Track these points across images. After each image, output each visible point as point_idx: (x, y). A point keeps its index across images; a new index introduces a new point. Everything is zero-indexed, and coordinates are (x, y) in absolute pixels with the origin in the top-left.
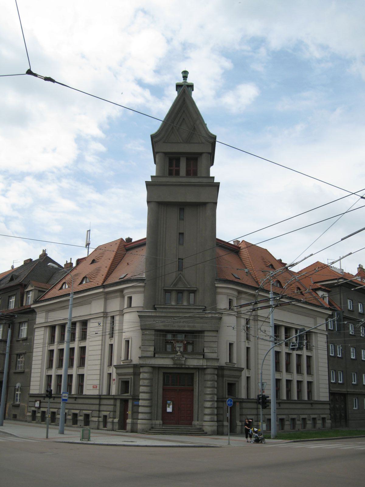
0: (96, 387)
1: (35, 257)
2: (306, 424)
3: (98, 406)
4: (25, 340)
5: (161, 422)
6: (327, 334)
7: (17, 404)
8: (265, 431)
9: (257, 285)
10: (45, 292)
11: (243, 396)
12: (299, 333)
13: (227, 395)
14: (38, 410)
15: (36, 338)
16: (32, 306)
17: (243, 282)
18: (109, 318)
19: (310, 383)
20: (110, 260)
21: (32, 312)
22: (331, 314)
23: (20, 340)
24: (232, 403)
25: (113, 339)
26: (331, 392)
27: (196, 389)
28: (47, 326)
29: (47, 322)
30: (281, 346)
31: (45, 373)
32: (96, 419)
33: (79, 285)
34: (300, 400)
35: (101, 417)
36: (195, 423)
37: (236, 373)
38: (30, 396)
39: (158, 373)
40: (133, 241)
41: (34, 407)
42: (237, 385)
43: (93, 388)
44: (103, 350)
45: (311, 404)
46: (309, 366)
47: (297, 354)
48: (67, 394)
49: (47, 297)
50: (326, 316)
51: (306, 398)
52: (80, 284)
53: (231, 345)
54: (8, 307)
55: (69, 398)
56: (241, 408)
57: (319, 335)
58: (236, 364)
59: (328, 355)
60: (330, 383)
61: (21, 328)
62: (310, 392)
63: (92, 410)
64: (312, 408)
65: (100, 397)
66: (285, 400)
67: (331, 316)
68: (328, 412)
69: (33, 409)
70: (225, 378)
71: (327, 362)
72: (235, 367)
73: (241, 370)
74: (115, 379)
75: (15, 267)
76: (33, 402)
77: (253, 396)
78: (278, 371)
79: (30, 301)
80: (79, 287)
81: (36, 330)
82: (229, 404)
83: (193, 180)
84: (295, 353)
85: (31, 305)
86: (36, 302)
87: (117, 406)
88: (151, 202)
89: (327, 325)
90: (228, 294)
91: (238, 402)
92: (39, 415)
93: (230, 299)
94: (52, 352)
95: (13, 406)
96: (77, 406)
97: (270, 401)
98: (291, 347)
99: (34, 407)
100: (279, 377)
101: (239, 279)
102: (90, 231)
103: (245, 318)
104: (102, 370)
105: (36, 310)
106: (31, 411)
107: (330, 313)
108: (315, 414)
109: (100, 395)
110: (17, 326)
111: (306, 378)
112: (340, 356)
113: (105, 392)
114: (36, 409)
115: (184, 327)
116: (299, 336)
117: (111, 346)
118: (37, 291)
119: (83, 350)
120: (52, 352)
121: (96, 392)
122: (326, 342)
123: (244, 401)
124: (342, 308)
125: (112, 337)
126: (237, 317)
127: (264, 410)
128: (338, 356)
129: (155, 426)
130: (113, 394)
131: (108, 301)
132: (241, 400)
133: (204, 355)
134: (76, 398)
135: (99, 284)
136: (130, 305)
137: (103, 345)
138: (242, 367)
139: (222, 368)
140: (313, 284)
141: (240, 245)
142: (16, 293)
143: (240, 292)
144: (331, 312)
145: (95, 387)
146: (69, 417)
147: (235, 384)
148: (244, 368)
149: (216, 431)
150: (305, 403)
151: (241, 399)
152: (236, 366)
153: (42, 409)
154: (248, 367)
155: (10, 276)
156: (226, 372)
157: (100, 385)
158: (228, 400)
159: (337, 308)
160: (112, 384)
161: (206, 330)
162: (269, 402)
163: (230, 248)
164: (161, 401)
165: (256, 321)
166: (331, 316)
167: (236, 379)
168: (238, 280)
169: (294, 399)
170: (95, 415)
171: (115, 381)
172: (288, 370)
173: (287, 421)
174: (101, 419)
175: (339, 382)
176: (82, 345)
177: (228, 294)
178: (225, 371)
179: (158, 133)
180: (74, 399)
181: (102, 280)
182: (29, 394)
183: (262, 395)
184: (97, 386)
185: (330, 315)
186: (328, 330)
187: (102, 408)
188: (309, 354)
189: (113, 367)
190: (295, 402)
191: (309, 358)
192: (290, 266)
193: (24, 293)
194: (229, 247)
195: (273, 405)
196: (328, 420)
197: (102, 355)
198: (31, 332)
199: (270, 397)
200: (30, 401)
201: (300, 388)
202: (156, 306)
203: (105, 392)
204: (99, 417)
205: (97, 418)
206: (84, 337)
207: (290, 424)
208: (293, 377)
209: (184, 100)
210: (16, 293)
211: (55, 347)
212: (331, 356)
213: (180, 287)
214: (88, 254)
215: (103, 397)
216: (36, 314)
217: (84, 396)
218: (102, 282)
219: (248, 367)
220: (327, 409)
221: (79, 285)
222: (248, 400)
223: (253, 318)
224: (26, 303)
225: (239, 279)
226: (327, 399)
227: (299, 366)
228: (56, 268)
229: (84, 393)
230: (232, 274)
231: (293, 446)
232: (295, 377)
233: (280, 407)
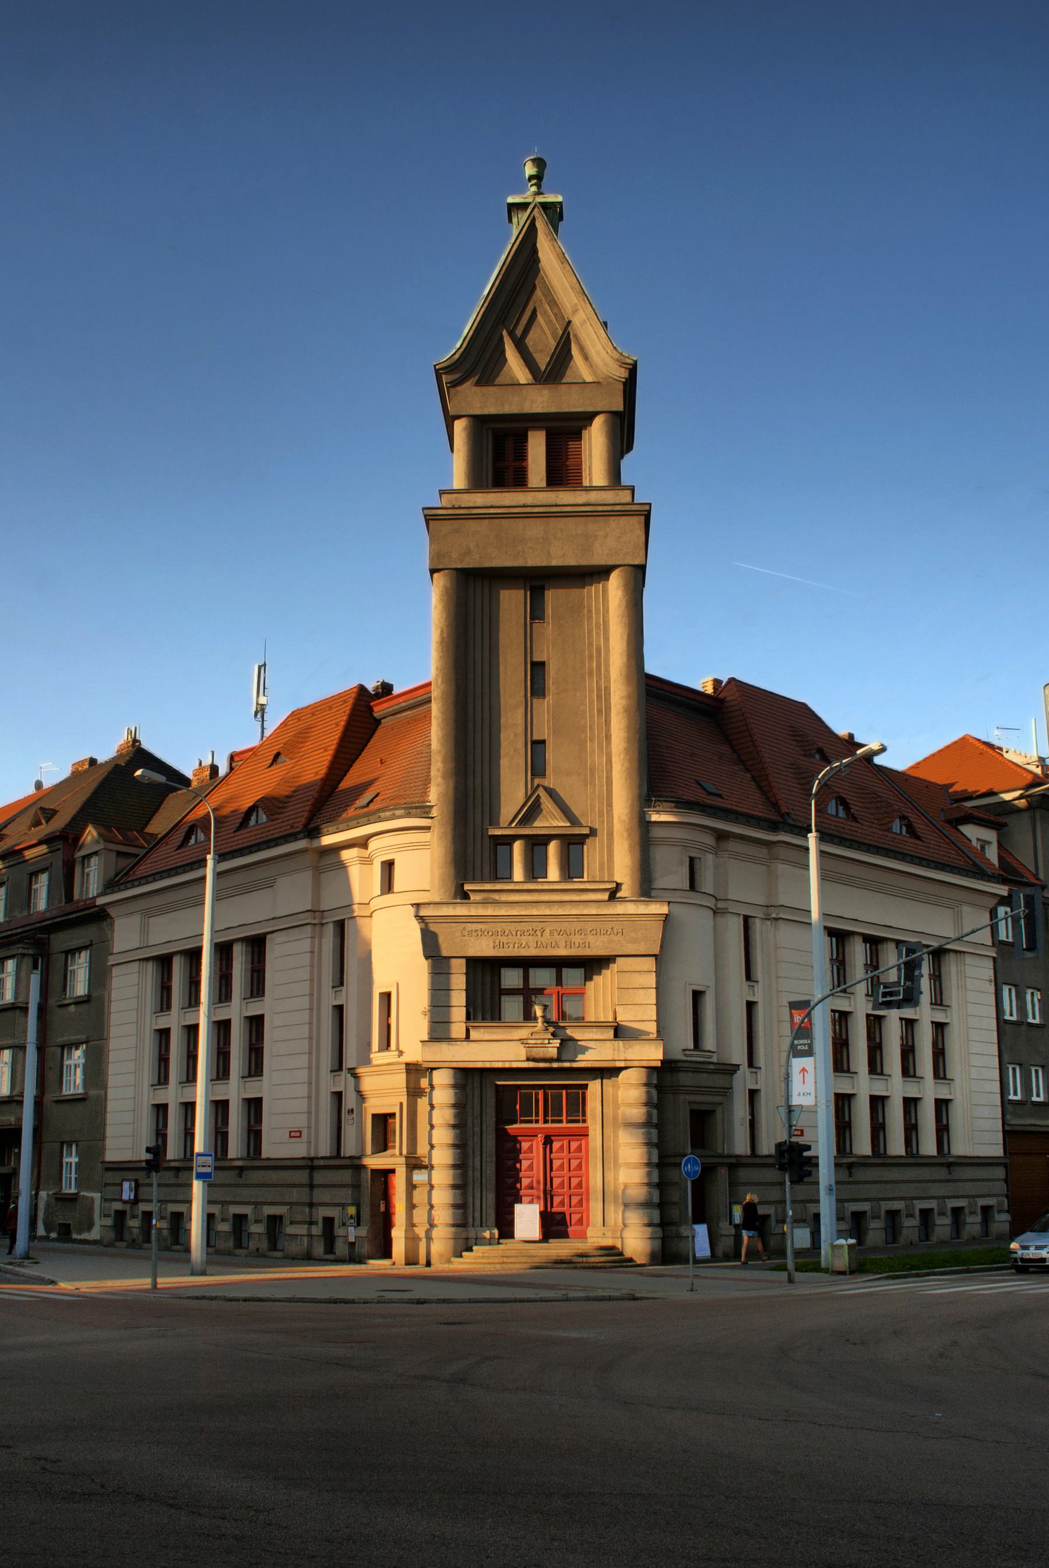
0: (298, 1134)
1: (106, 752)
3: (307, 1190)
4: (80, 1002)
6: (995, 955)
7: (73, 1194)
8: (809, 1249)
9: (776, 814)
10: (138, 855)
11: (741, 1146)
12: (907, 956)
13: (690, 1147)
14: (131, 1208)
15: (114, 995)
16: (100, 901)
17: (730, 807)
18: (330, 930)
19: (942, 1105)
20: (326, 753)
21: (99, 916)
22: (1005, 894)
23: (69, 1005)
24: (698, 1169)
25: (344, 988)
26: (1007, 1128)
28: (147, 959)
29: (145, 945)
30: (851, 996)
31: (149, 1098)
32: (302, 1230)
33: (235, 832)
34: (913, 1156)
35: (316, 1223)
37: (719, 1081)
38: (107, 1169)
39: (481, 1085)
40: (396, 691)
41: (121, 1200)
42: (719, 1115)
43: (290, 1137)
44: (314, 1024)
45: (949, 1165)
46: (939, 1053)
47: (901, 1019)
48: (210, 1158)
49: (142, 870)
50: (992, 902)
51: (928, 1146)
52: (239, 828)
53: (697, 996)
54: (29, 907)
55: (216, 1168)
56: (733, 1184)
57: (969, 959)
58: (714, 1052)
59: (998, 1019)
60: (1005, 1103)
61: (70, 968)
62: (943, 1130)
63: (291, 1204)
64: (950, 1177)
65: (311, 1164)
66: (869, 1157)
67: (1005, 901)
68: (1001, 1187)
69: (117, 1206)
71: (995, 1040)
72: (712, 1063)
73: (734, 1068)
74: (352, 1110)
75: (47, 784)
76: (114, 1184)
77: (767, 1147)
78: (843, 1071)
79: (94, 887)
80: (237, 838)
81: (115, 971)
82: (690, 1173)
83: (565, 497)
84: (893, 1017)
85: (94, 898)
86: (111, 885)
87: (362, 1188)
89: (994, 930)
90: (684, 845)
91: (723, 1164)
92: (134, 1223)
93: (692, 860)
94: (164, 1034)
95: (57, 1199)
96: (245, 1193)
97: (814, 1161)
98: (881, 1000)
99: (121, 1200)
100: (847, 1090)
101: (720, 796)
102: (265, 665)
103: (739, 914)
104: (313, 1084)
105: (111, 911)
106: (113, 1213)
107: (1003, 890)
108: (958, 1197)
109: (311, 1159)
110: (58, 960)
111: (929, 1090)
112: (1037, 1021)
113: (325, 1149)
114: (127, 1207)
116: (905, 963)
117: (339, 1009)
118: (115, 854)
119: (256, 1024)
120: (164, 1034)
121: (298, 1150)
122: (990, 981)
123: (744, 1161)
124: (1041, 876)
125: (342, 984)
126: (715, 913)
127: (797, 1187)
128: (1030, 1020)
130: (348, 1155)
131: (323, 876)
132: (733, 1161)
134: (241, 1169)
135: (295, 825)
136: (388, 885)
137: (314, 1009)
138: (735, 1061)
139: (673, 1065)
140: (950, 806)
141: (721, 691)
142: (52, 863)
143: (721, 836)
144: (1007, 888)
145: (295, 1134)
146: (225, 1227)
147: (712, 1112)
148: (739, 1065)
149: (158, 1275)
150: (927, 1162)
151: (731, 1156)
152: (714, 1059)
153: (143, 1207)
154: (751, 1063)
155: (31, 813)
157: (309, 1127)
158: (686, 1160)
159: (1025, 875)
160: (345, 1125)
162: (813, 1162)
163: (687, 701)
164: (494, 1168)
166: (1005, 901)
167: (717, 1099)
168: (715, 798)
170: (299, 1218)
171: (354, 1115)
172: (875, 1067)
173: (873, 1218)
174: (317, 1230)
175: (1035, 1099)
176: (254, 1010)
177: (684, 845)
180: (236, 1172)
181: (306, 814)
182: (103, 1162)
183: (790, 1142)
184: (300, 1132)
185: (1003, 897)
186: (997, 943)
187: (320, 1195)
188: (940, 1017)
189: (346, 1076)
190: (896, 1163)
191: (939, 1028)
192: (546, 789)
193: (74, 861)
194: (683, 699)
195: (825, 1174)
196: (999, 1212)
197: (313, 1038)
198: (99, 977)
199: (813, 1147)
200: (106, 1185)
201: (945, 1122)
202: (467, 887)
203: (325, 1149)
204: (311, 1223)
205: (306, 1226)
206: (257, 987)
207: (850, 1230)
208: (889, 1088)
210: (52, 863)
211: (174, 1021)
212: (1007, 1022)
213: (543, 825)
214: (262, 736)
215: (322, 1163)
216: (112, 924)
217: (265, 1163)
218: (303, 820)
219: (751, 1063)
220: (999, 1180)
221: (235, 832)
222: (755, 1161)
223: (765, 914)
224: (82, 892)
225: (720, 796)
226: (998, 1151)
227: (908, 1052)
228: (160, 784)
229: (264, 1155)
230: (698, 783)
231: (920, 1291)
232: (896, 1088)
233: (851, 1179)
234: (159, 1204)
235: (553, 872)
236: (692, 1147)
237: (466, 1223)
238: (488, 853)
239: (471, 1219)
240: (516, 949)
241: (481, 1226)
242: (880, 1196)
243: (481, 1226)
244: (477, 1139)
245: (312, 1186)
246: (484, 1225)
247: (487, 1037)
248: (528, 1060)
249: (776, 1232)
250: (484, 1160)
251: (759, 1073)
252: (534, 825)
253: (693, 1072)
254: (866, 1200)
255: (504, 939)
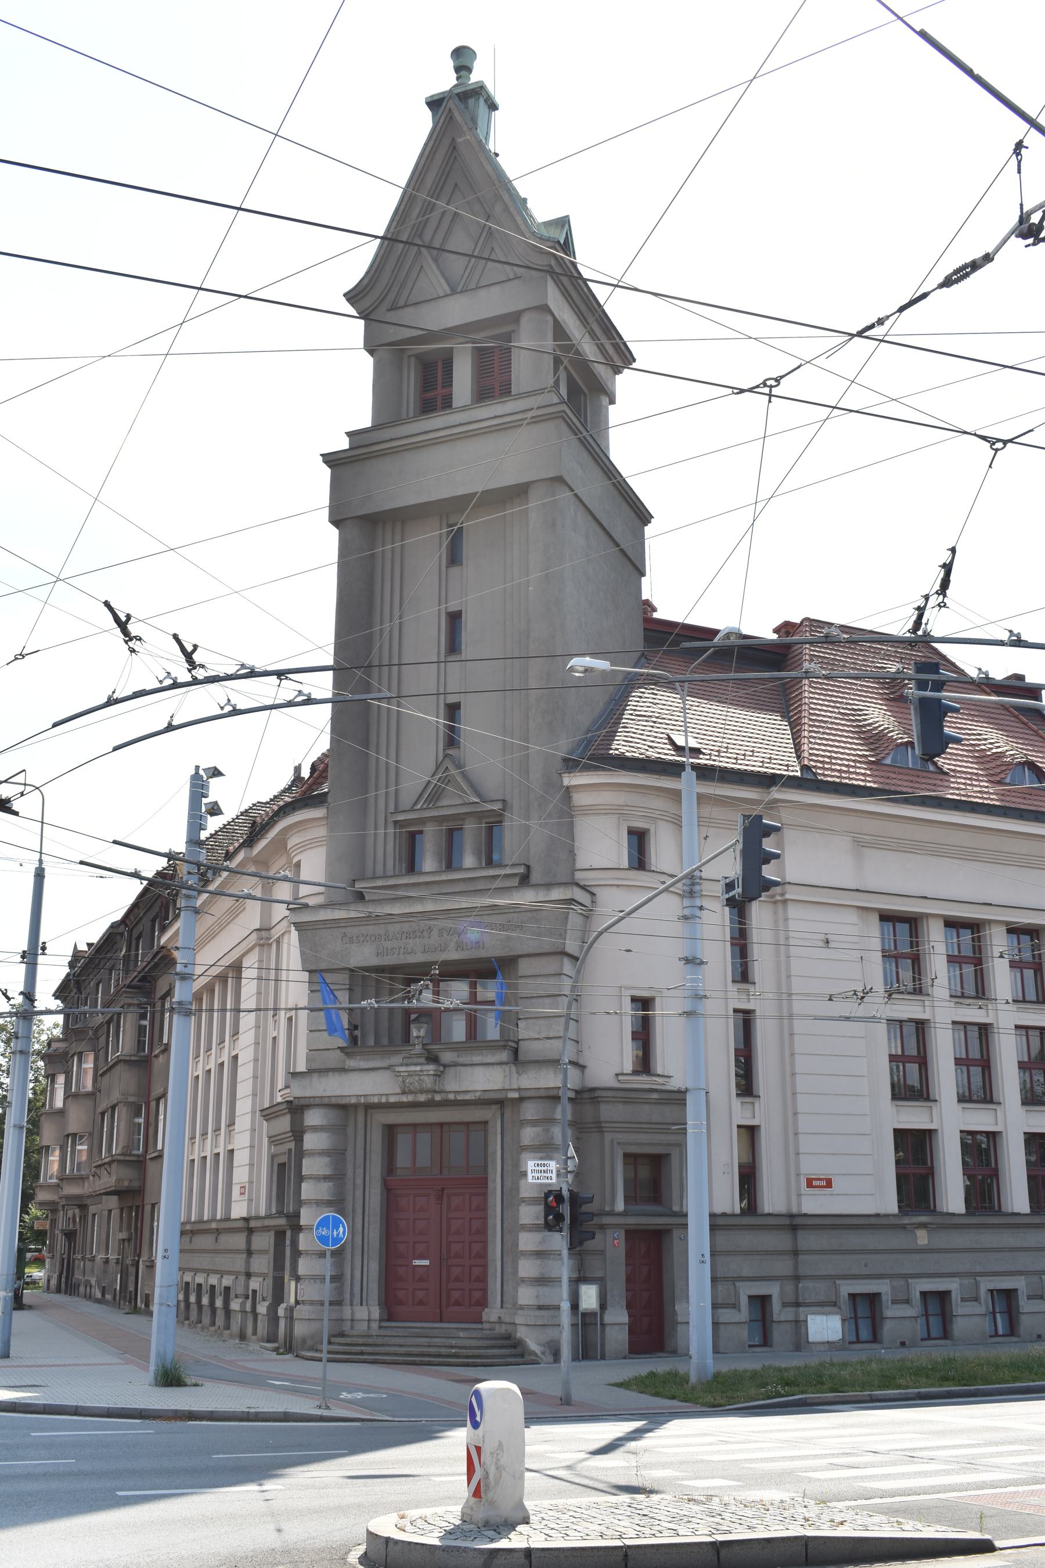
2: (883, 1318)
5: (376, 1313)
27: (494, 1181)
36: (492, 1313)
37: (669, 1113)
66: (894, 1215)
70: (608, 1137)
88: (346, 519)
90: (619, 812)
109: (791, 1216)
115: (413, 952)
118: (875, 918)
122: (296, 1005)
129: (352, 1328)
133: (516, 1052)
147: (667, 1156)
156: (608, 1112)
161: (521, 953)
165: (780, 906)
169: (945, 1211)
177: (619, 812)
178: (603, 1107)
179: (366, 281)
209: (454, 147)
234: (181, 1273)
235: (469, 860)
236: (627, 1199)
237: (342, 1301)
238: (392, 844)
239: (347, 1296)
240: (402, 956)
241: (361, 1305)
242: (978, 1269)
243: (361, 1305)
244: (359, 1194)
245: (796, 1253)
246: (364, 1303)
247: (363, 1064)
248: (404, 1093)
249: (783, 1318)
250: (366, 1219)
251: (757, 1105)
252: (440, 804)
253: (625, 1103)
254: (1020, 1273)
255: (388, 944)
